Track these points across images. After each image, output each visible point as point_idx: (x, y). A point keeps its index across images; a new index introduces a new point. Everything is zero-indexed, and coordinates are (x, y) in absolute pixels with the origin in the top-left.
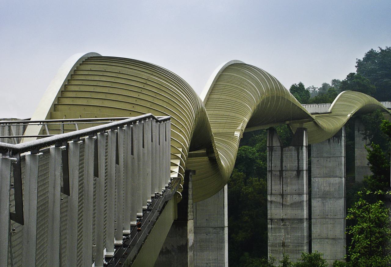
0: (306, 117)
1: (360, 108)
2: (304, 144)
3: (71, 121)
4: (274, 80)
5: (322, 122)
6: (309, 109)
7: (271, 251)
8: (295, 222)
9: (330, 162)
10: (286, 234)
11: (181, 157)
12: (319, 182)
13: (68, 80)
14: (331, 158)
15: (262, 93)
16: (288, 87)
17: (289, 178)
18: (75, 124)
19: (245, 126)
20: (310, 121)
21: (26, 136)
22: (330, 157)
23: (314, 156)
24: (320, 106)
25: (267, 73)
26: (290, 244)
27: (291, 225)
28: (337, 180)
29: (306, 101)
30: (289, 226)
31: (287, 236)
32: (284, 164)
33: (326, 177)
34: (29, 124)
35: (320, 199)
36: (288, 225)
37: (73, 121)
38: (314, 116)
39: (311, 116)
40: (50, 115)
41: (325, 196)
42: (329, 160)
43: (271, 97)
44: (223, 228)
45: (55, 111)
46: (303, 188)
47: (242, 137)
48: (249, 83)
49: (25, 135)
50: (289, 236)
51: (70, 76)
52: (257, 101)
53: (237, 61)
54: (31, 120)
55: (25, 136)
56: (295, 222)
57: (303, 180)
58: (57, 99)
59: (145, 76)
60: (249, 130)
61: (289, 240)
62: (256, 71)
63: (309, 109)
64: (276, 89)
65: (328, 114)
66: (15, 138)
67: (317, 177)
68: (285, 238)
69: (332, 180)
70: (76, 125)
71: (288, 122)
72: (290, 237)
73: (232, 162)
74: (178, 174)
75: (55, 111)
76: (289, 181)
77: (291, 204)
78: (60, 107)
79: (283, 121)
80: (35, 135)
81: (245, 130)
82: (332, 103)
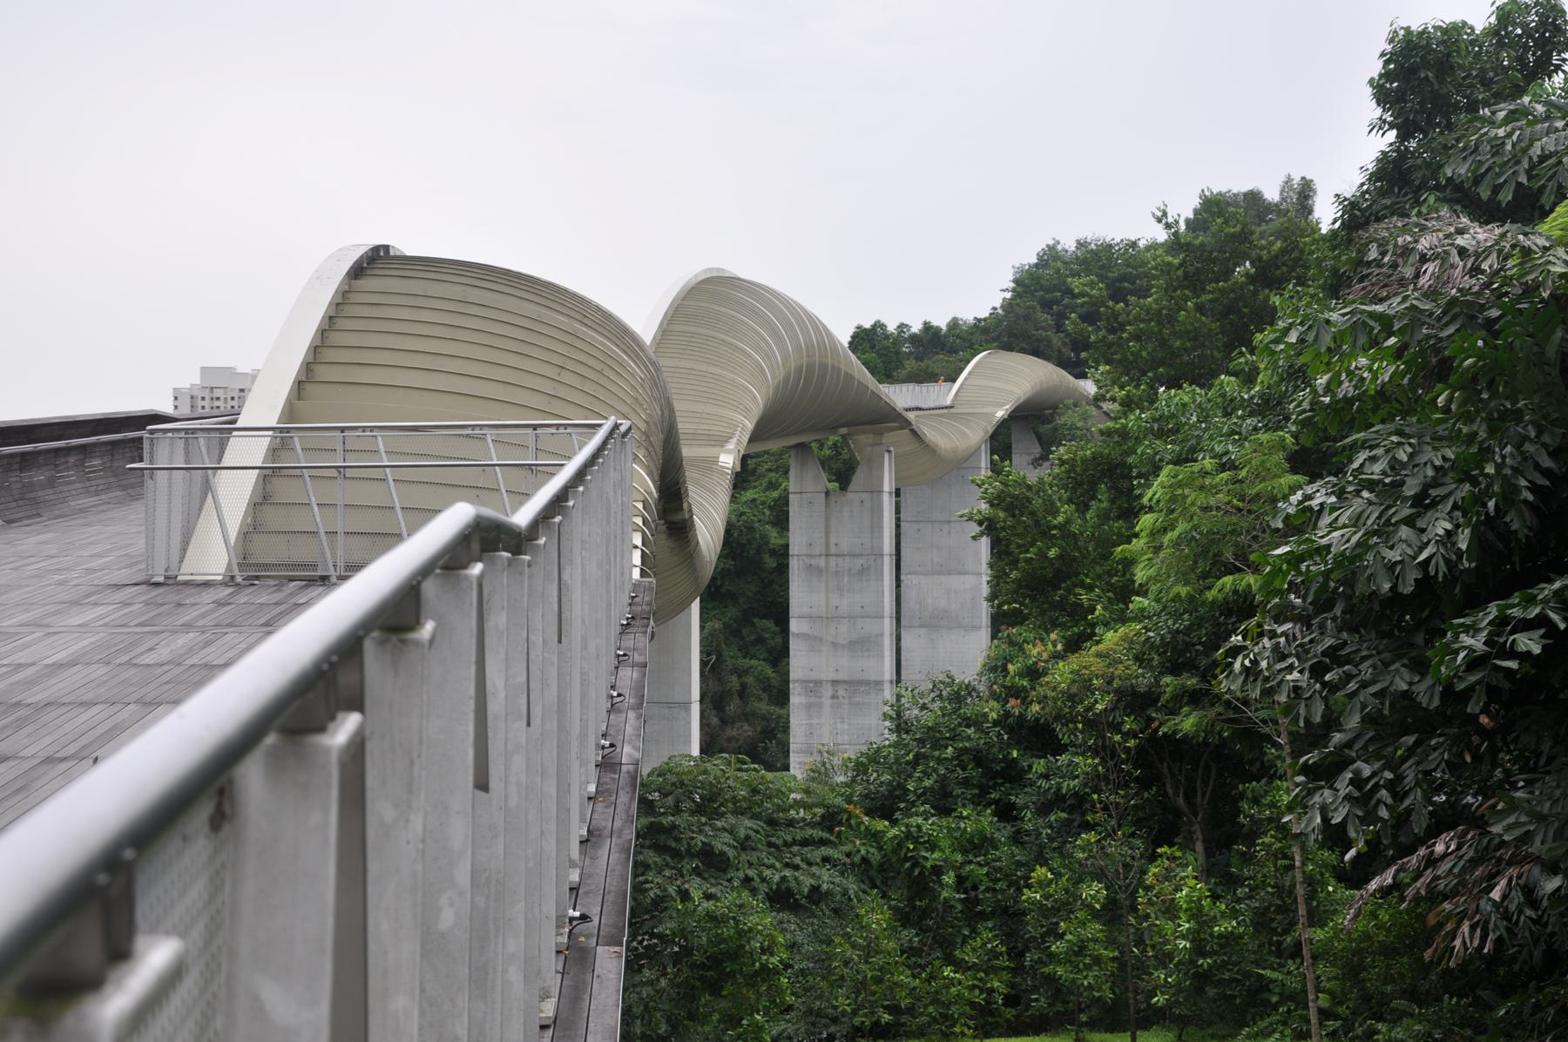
0: (889, 418)
1: (1028, 395)
2: (886, 488)
3: (364, 429)
4: (813, 320)
5: (930, 433)
6: (901, 396)
7: (797, 766)
8: (862, 689)
9: (949, 533)
10: (838, 721)
11: (644, 524)
12: (923, 590)
13: (330, 317)
14: (952, 524)
15: (785, 357)
16: (844, 337)
17: (846, 573)
18: (376, 436)
19: (745, 440)
20: (902, 428)
21: (229, 465)
22: (950, 522)
23: (909, 519)
24: (924, 389)
25: (797, 304)
26: (847, 747)
27: (849, 697)
28: (969, 581)
29: (887, 373)
30: (846, 701)
31: (839, 726)
32: (833, 540)
33: (940, 573)
34: (235, 433)
35: (923, 630)
36: (843, 697)
37: (372, 429)
38: (911, 416)
39: (906, 414)
40: (290, 412)
41: (936, 622)
42: (946, 528)
43: (807, 366)
44: (686, 705)
45: (299, 398)
46: (883, 602)
47: (739, 469)
48: (751, 328)
49: (226, 462)
50: (846, 727)
51: (334, 307)
52: (774, 377)
53: (718, 270)
54: (238, 425)
55: (225, 465)
56: (862, 689)
57: (882, 580)
58: (305, 365)
59: (532, 310)
60: (758, 448)
61: (846, 737)
62: (769, 299)
63: (901, 396)
64: (819, 345)
65: (945, 411)
66: (388, 470)
67: (915, 573)
68: (835, 732)
69: (956, 581)
70: (380, 439)
71: (843, 431)
72: (849, 730)
73: (715, 538)
74: (642, 569)
75: (299, 399)
76: (846, 581)
77: (851, 642)
78: (309, 387)
79: (833, 428)
80: (254, 465)
81: (745, 450)
82: (954, 381)
